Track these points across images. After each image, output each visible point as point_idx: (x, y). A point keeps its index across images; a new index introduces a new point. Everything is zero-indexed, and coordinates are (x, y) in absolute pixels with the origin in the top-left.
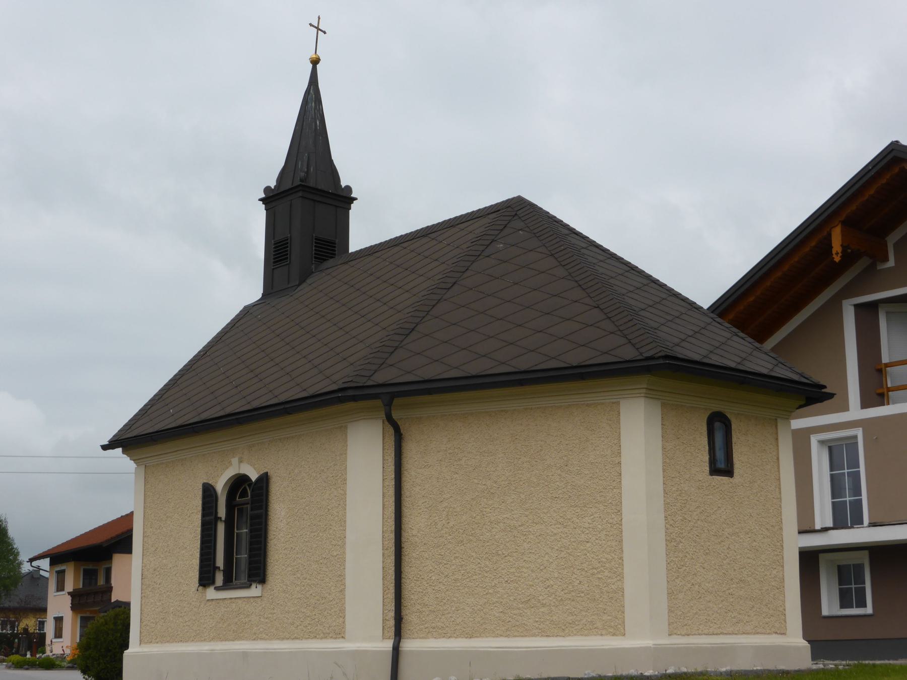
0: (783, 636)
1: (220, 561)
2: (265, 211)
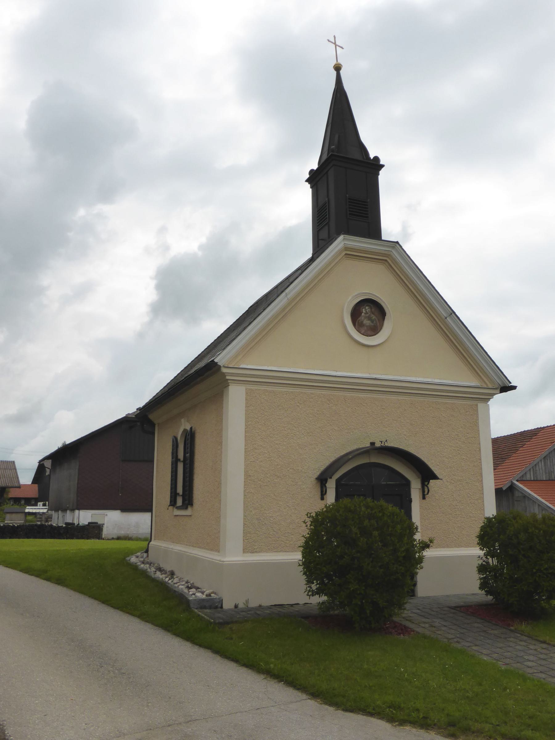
0: (421, 497)
1: (180, 490)
2: (311, 189)
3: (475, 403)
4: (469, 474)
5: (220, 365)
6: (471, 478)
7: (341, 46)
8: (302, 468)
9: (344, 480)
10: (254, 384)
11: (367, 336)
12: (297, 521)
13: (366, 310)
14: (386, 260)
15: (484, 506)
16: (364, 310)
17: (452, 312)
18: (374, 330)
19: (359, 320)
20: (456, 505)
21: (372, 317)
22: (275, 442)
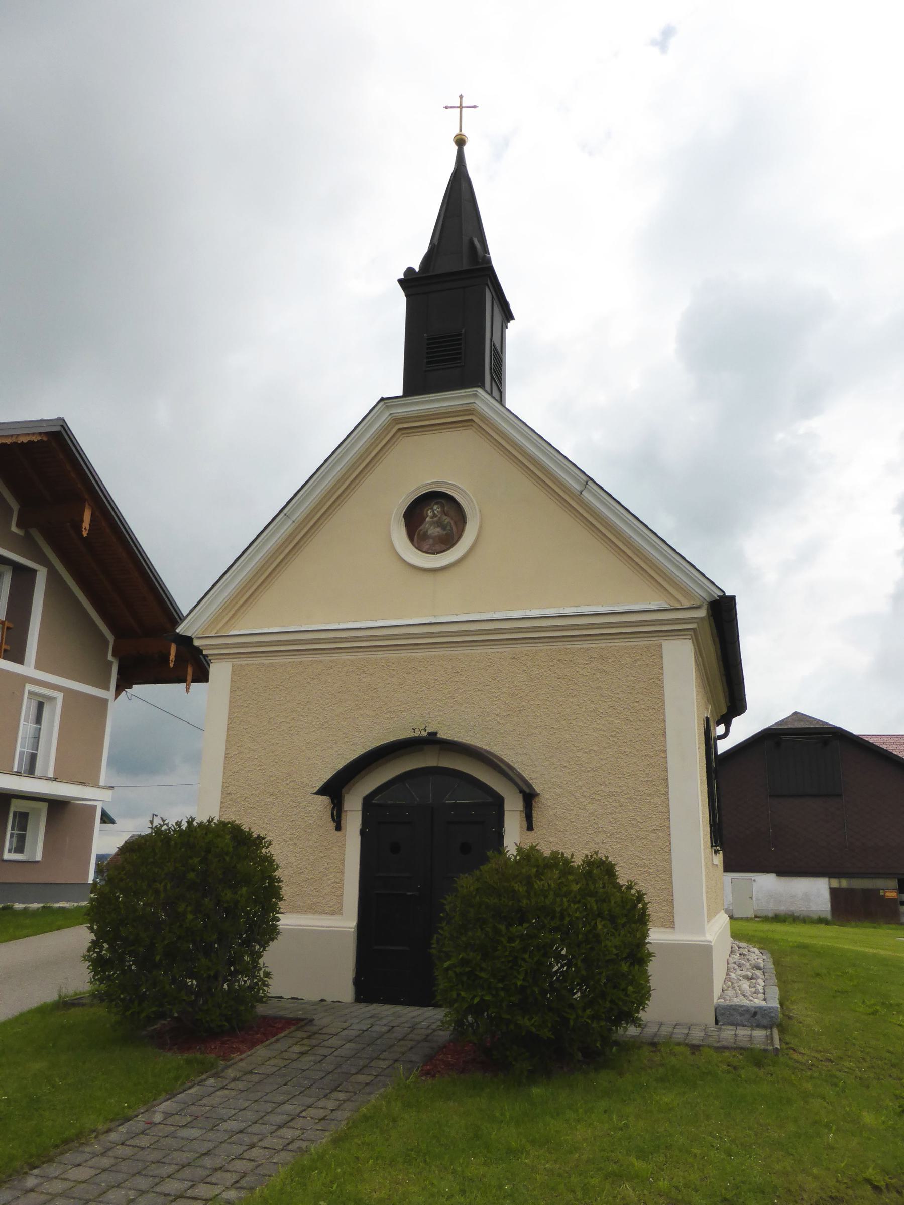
0: (525, 824)
3: (655, 641)
4: (636, 782)
5: (190, 637)
6: (640, 789)
7: (473, 105)
8: (308, 779)
9: (376, 798)
10: (245, 658)
11: (433, 554)
12: (295, 863)
13: (434, 511)
14: (471, 420)
15: (670, 844)
16: (431, 512)
17: (588, 479)
18: (448, 541)
19: (421, 530)
20: (603, 843)
21: (444, 521)
22: (270, 742)
